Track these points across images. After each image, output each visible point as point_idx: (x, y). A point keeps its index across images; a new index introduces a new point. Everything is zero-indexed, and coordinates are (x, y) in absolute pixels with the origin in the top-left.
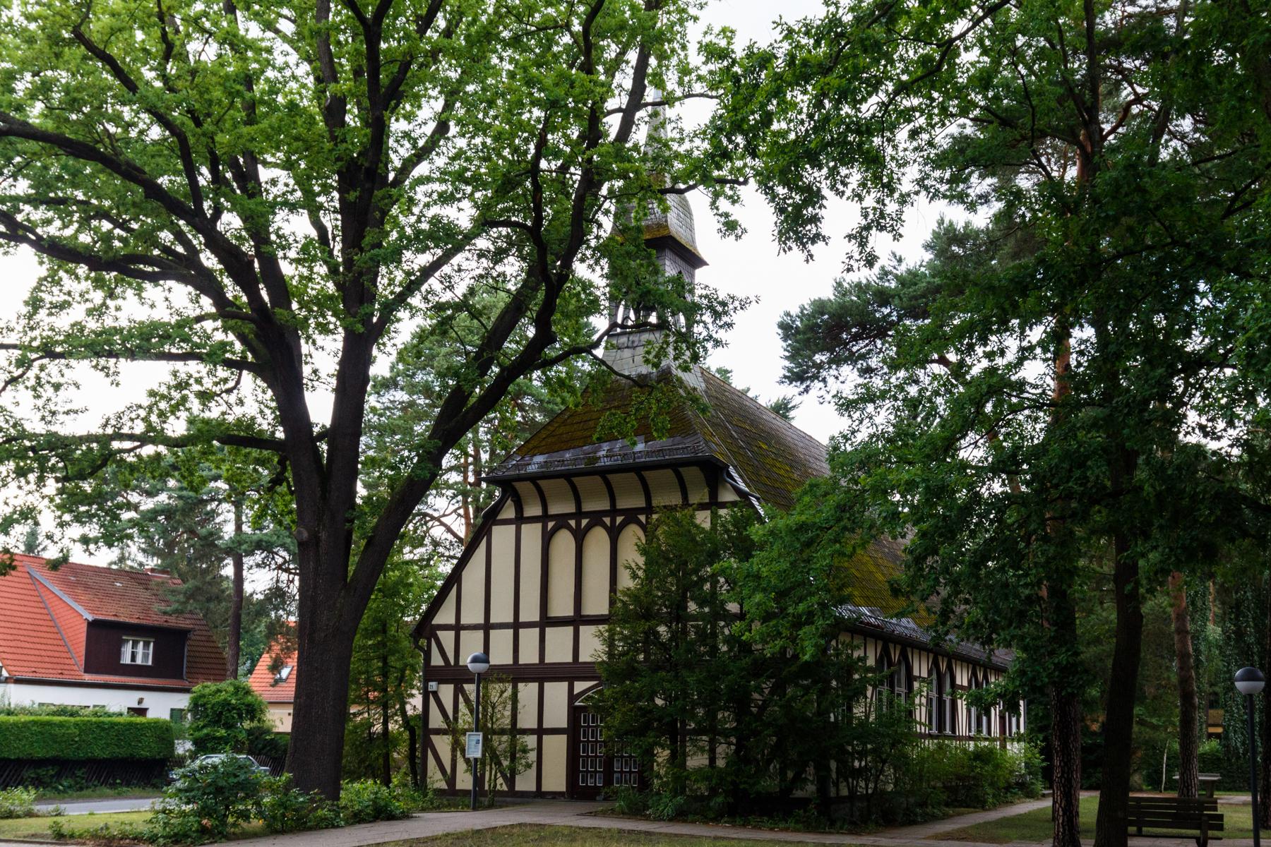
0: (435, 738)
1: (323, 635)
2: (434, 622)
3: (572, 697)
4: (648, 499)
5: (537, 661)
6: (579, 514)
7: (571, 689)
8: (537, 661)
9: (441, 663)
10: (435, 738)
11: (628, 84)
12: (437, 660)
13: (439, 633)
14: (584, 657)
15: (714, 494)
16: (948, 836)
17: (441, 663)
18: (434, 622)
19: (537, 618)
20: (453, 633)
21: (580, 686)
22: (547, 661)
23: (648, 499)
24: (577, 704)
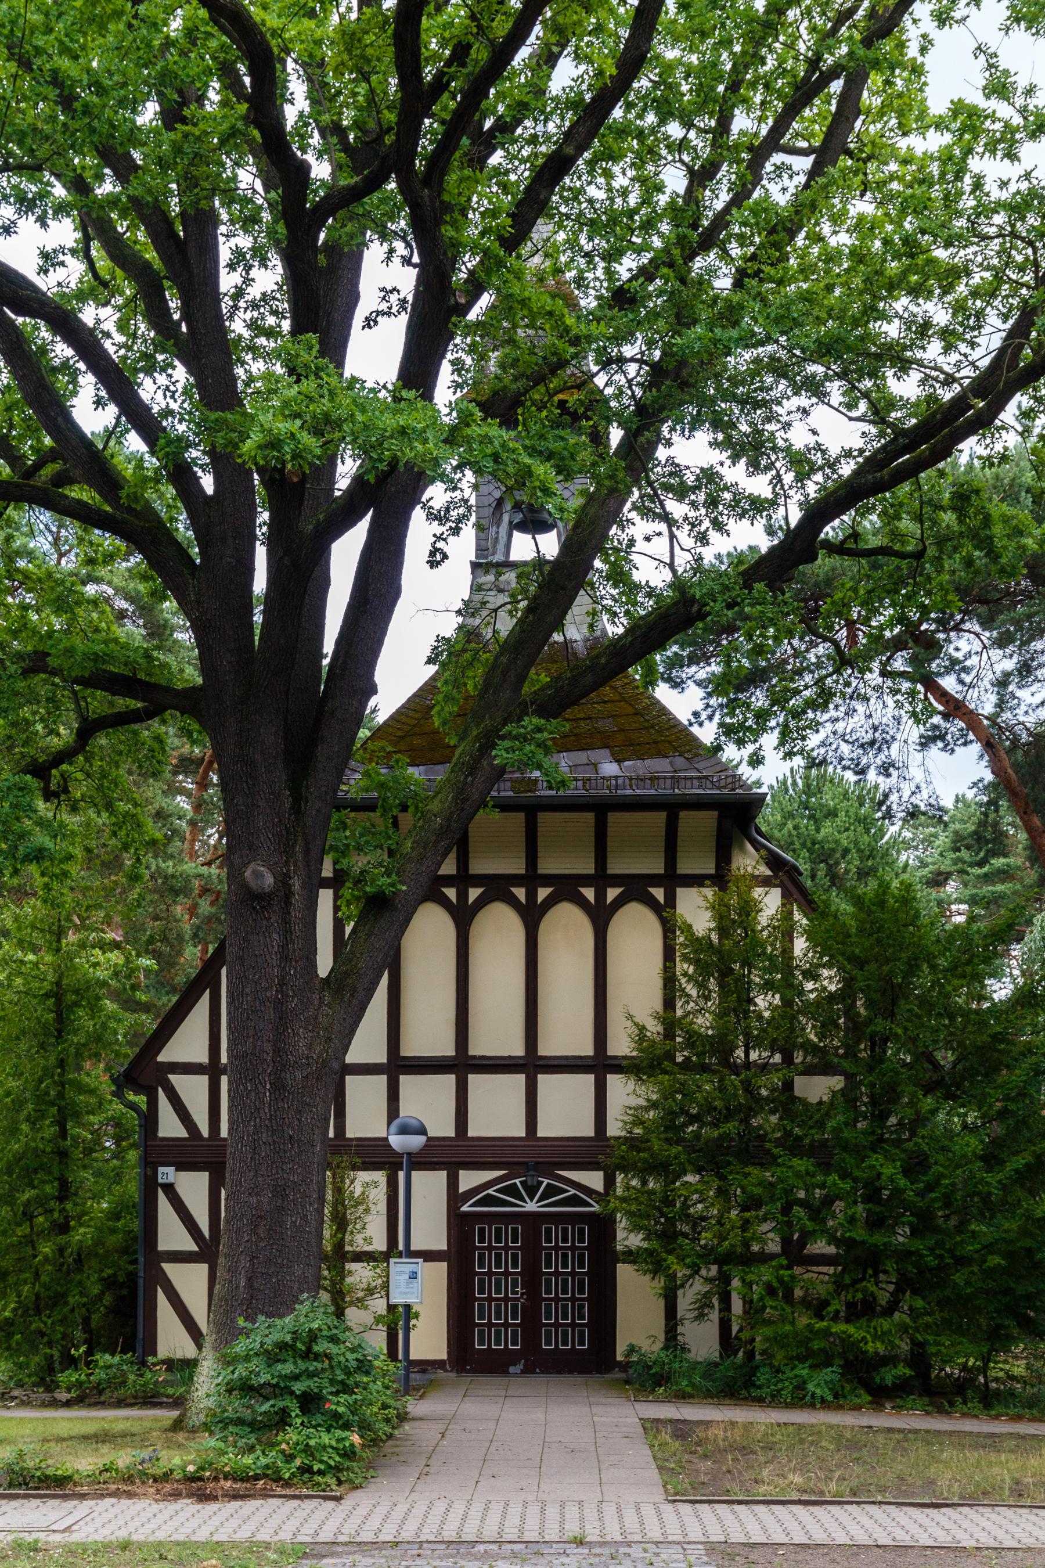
0: (170, 1269)
1: (299, 1075)
2: (161, 1058)
3: (455, 1198)
4: (532, 857)
5: (590, 1132)
6: (532, 879)
7: (453, 1183)
8: (590, 1132)
9: (182, 1133)
10: (170, 1269)
11: (521, 175)
12: (170, 1126)
13: (173, 1078)
14: (614, 1129)
15: (724, 857)
16: (69, 1419)
17: (182, 1133)
18: (161, 1058)
19: (382, 1058)
20: (204, 1080)
21: (468, 1180)
22: (540, 1134)
23: (532, 857)
24: (465, 1208)
